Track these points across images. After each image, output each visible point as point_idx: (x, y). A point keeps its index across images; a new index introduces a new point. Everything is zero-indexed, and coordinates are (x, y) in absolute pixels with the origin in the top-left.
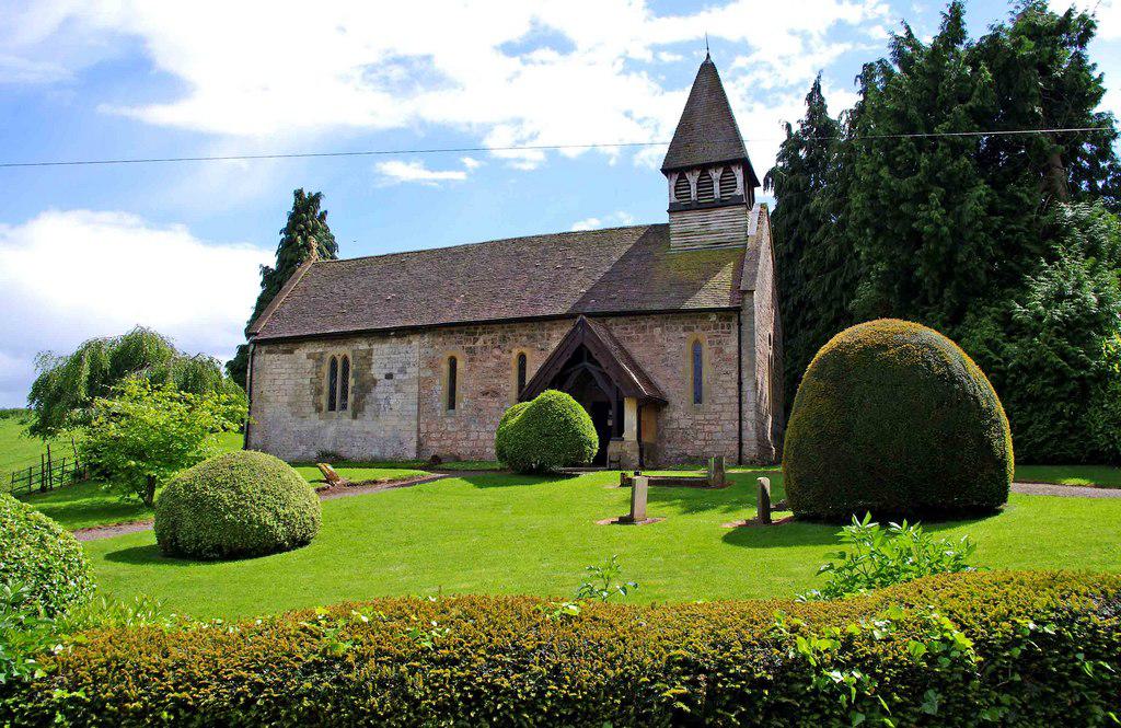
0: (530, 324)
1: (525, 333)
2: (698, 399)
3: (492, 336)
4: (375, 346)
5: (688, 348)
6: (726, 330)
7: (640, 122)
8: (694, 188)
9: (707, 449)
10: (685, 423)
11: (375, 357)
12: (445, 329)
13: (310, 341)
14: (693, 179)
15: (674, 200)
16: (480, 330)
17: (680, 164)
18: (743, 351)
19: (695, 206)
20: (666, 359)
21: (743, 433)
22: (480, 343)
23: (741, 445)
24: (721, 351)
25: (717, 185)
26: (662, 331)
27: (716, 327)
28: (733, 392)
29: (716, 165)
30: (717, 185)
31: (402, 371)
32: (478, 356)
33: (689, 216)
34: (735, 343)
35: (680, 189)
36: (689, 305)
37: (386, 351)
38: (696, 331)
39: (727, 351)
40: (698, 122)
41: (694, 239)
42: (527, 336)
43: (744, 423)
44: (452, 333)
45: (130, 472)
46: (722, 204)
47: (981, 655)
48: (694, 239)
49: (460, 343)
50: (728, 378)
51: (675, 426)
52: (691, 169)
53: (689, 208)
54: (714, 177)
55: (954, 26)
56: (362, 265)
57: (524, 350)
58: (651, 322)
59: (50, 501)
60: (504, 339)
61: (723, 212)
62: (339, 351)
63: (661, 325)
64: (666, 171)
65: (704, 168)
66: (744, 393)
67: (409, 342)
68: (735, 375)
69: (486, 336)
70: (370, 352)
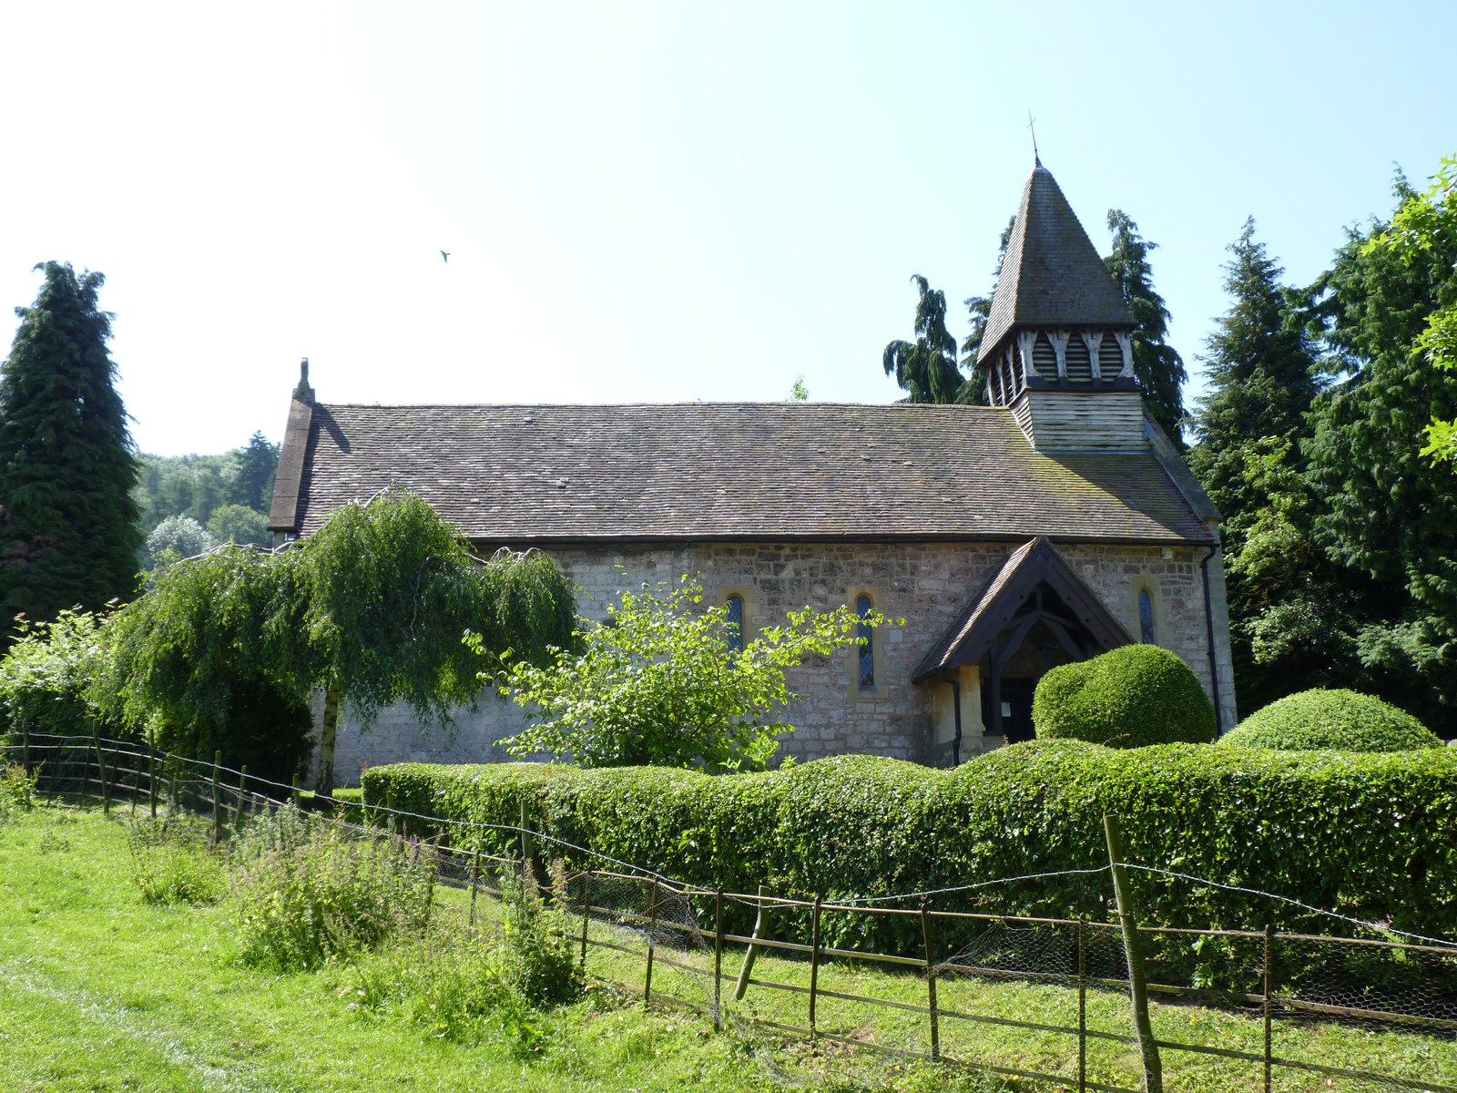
0: (879, 546)
1: (868, 561)
3: (811, 562)
4: (577, 569)
6: (1185, 574)
8: (1060, 357)
12: (719, 546)
16: (787, 551)
17: (1044, 318)
18: (1213, 607)
22: (787, 573)
24: (1181, 604)
26: (1096, 569)
27: (1171, 569)
29: (1093, 328)
30: (1095, 358)
32: (787, 595)
33: (1058, 399)
34: (1200, 593)
37: (601, 578)
39: (1190, 605)
42: (873, 565)
44: (731, 552)
45: (68, 774)
46: (1106, 388)
47: (434, 679)
48: (1069, 436)
50: (1193, 645)
52: (1056, 328)
55: (6, 398)
57: (868, 590)
60: (831, 569)
61: (1110, 399)
63: (1094, 561)
65: (1076, 331)
66: (1218, 668)
67: (651, 565)
68: (1203, 641)
69: (800, 563)
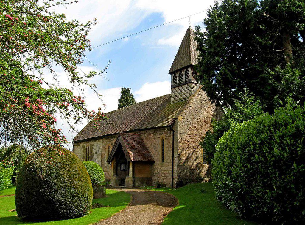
2: (163, 161)
5: (160, 140)
7: (91, 86)
9: (164, 180)
10: (159, 170)
11: (94, 146)
13: (83, 142)
14: (177, 75)
15: (173, 84)
19: (178, 85)
20: (154, 146)
21: (174, 174)
23: (173, 179)
25: (184, 76)
28: (171, 158)
31: (99, 151)
35: (174, 79)
36: (159, 125)
38: (162, 134)
40: (181, 55)
41: (177, 98)
43: (174, 170)
49: (110, 141)
51: (156, 171)
53: (180, 85)
54: (183, 73)
56: (139, 103)
58: (150, 132)
59: (147, 190)
62: (88, 145)
63: (153, 133)
64: (170, 73)
66: (174, 159)
70: (93, 145)
